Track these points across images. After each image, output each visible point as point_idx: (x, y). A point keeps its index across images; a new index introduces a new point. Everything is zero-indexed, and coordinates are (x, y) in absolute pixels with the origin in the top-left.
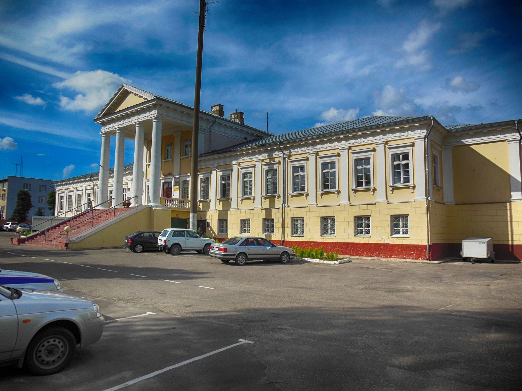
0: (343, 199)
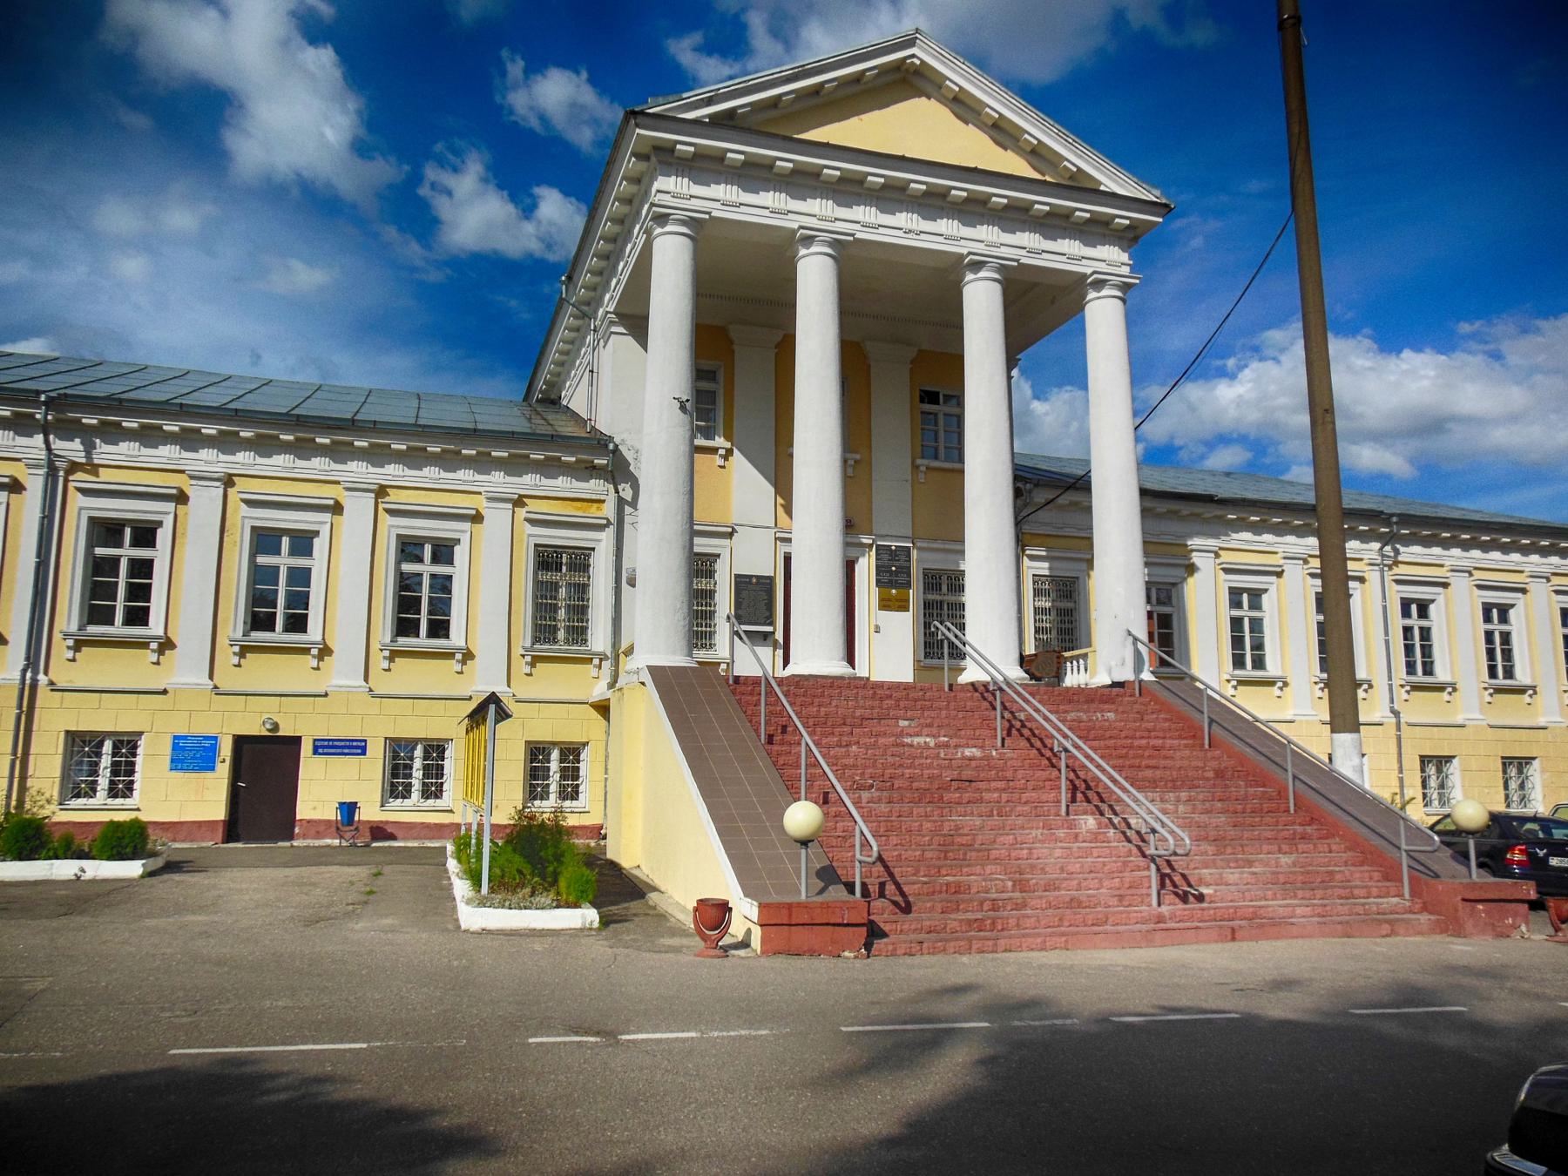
0: (342, 673)
